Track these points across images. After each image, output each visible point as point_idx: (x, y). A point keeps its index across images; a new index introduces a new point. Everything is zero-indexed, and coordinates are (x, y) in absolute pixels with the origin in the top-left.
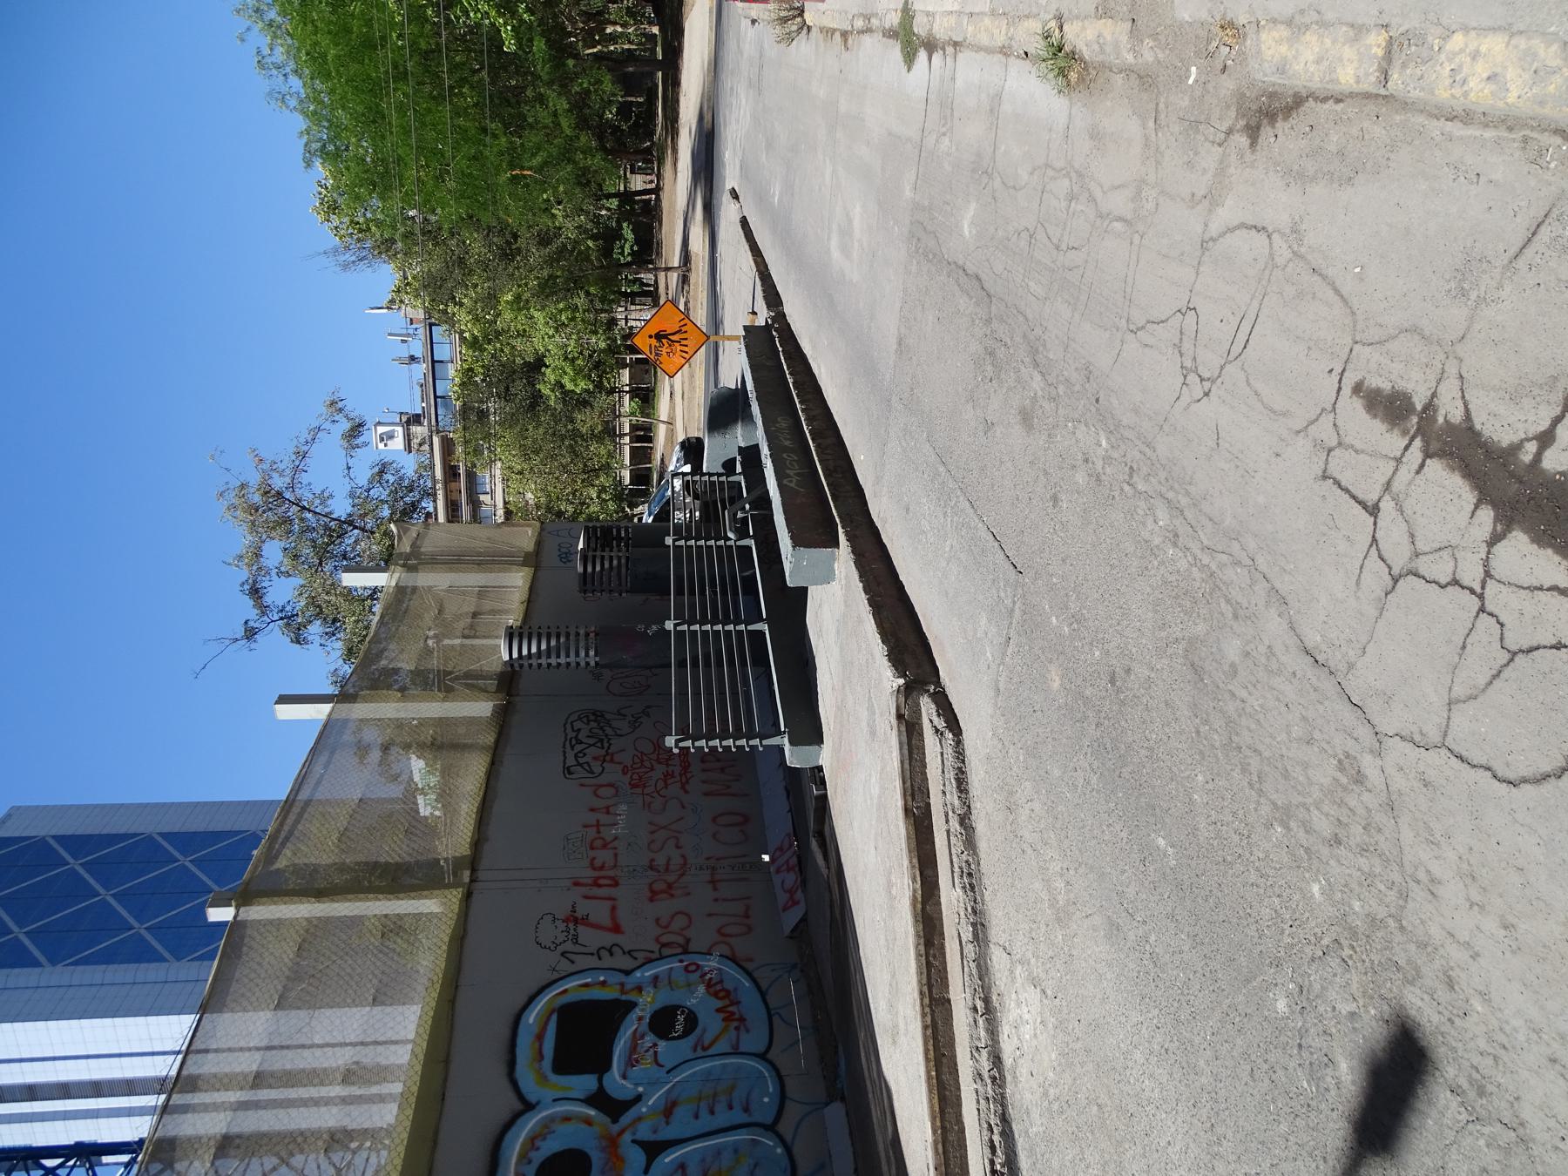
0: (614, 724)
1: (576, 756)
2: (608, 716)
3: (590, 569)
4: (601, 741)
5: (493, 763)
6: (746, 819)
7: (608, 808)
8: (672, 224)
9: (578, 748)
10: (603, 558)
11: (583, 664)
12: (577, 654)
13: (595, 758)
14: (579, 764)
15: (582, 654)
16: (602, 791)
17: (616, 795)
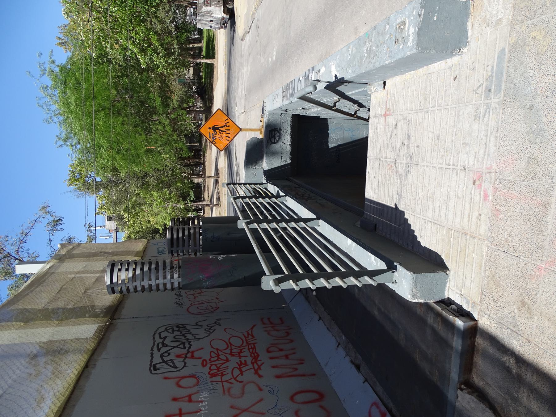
0: (193, 332)
1: (162, 356)
2: (188, 327)
3: (175, 236)
4: (184, 343)
5: (86, 366)
6: (321, 396)
7: (190, 396)
8: (211, 168)
9: (163, 350)
10: (184, 230)
11: (169, 286)
12: (165, 277)
13: (178, 356)
14: (164, 362)
15: (169, 277)
16: (183, 383)
17: (198, 384)
